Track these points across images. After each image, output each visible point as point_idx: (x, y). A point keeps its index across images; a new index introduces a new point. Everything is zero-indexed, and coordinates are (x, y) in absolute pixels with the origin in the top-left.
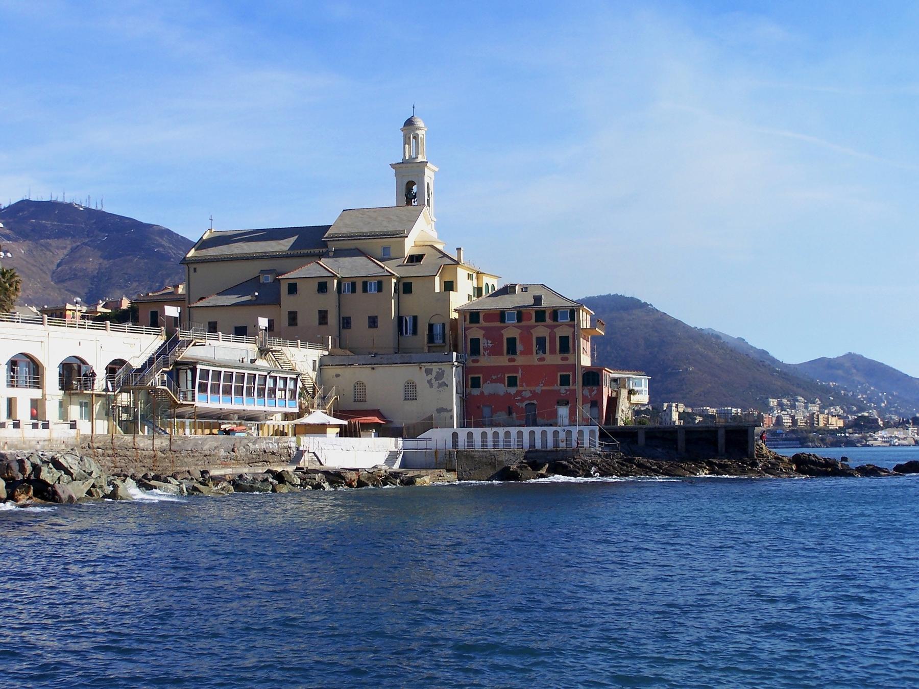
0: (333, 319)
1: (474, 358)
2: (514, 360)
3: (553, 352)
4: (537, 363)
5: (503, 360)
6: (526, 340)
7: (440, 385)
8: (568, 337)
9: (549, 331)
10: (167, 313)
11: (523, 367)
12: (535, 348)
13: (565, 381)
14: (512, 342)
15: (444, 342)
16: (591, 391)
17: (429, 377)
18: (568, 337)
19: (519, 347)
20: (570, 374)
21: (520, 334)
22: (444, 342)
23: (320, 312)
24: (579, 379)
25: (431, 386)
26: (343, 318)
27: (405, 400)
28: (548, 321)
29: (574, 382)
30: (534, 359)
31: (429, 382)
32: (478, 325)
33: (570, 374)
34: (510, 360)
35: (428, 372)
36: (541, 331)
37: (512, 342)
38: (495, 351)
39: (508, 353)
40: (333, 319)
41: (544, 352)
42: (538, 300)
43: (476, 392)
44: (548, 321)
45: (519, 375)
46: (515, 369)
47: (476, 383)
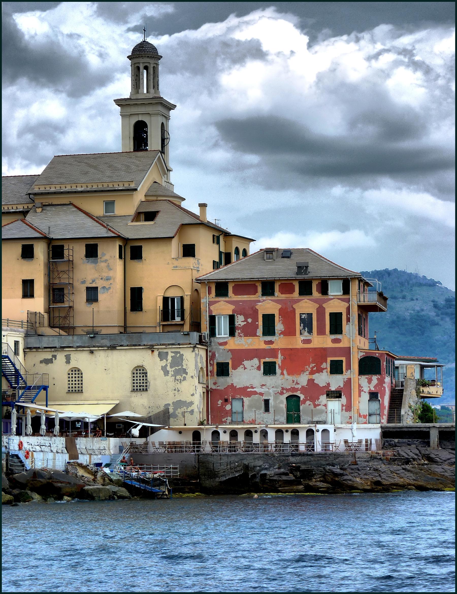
0: (39, 289)
1: (268, 338)
2: (271, 342)
3: (321, 332)
4: (300, 345)
5: (258, 342)
6: (288, 314)
7: (177, 373)
8: (341, 314)
9: (317, 306)
10: (452, 84)
11: (284, 351)
12: (298, 326)
13: (336, 368)
14: (269, 320)
15: (183, 319)
16: (370, 381)
17: (163, 363)
18: (341, 314)
19: (279, 326)
20: (344, 359)
21: (280, 310)
22: (183, 319)
23: (32, 296)
24: (355, 366)
25: (166, 373)
26: (133, 289)
27: (133, 390)
28: (316, 294)
29: (349, 367)
30: (298, 342)
31: (164, 369)
32: (227, 299)
33: (344, 359)
34: (336, 341)
35: (162, 356)
36: (306, 306)
37: (269, 320)
38: (249, 331)
39: (332, 332)
40: (39, 289)
41: (310, 332)
42: (302, 268)
43: (223, 382)
44: (316, 294)
45: (279, 361)
46: (274, 353)
47: (223, 370)
